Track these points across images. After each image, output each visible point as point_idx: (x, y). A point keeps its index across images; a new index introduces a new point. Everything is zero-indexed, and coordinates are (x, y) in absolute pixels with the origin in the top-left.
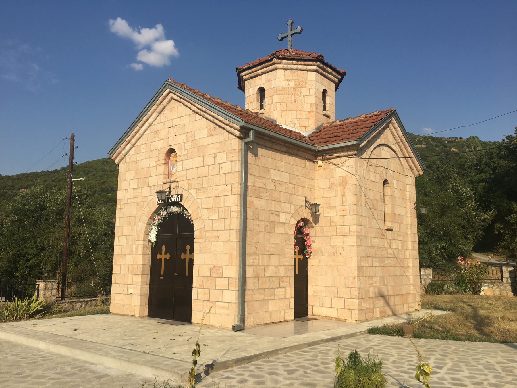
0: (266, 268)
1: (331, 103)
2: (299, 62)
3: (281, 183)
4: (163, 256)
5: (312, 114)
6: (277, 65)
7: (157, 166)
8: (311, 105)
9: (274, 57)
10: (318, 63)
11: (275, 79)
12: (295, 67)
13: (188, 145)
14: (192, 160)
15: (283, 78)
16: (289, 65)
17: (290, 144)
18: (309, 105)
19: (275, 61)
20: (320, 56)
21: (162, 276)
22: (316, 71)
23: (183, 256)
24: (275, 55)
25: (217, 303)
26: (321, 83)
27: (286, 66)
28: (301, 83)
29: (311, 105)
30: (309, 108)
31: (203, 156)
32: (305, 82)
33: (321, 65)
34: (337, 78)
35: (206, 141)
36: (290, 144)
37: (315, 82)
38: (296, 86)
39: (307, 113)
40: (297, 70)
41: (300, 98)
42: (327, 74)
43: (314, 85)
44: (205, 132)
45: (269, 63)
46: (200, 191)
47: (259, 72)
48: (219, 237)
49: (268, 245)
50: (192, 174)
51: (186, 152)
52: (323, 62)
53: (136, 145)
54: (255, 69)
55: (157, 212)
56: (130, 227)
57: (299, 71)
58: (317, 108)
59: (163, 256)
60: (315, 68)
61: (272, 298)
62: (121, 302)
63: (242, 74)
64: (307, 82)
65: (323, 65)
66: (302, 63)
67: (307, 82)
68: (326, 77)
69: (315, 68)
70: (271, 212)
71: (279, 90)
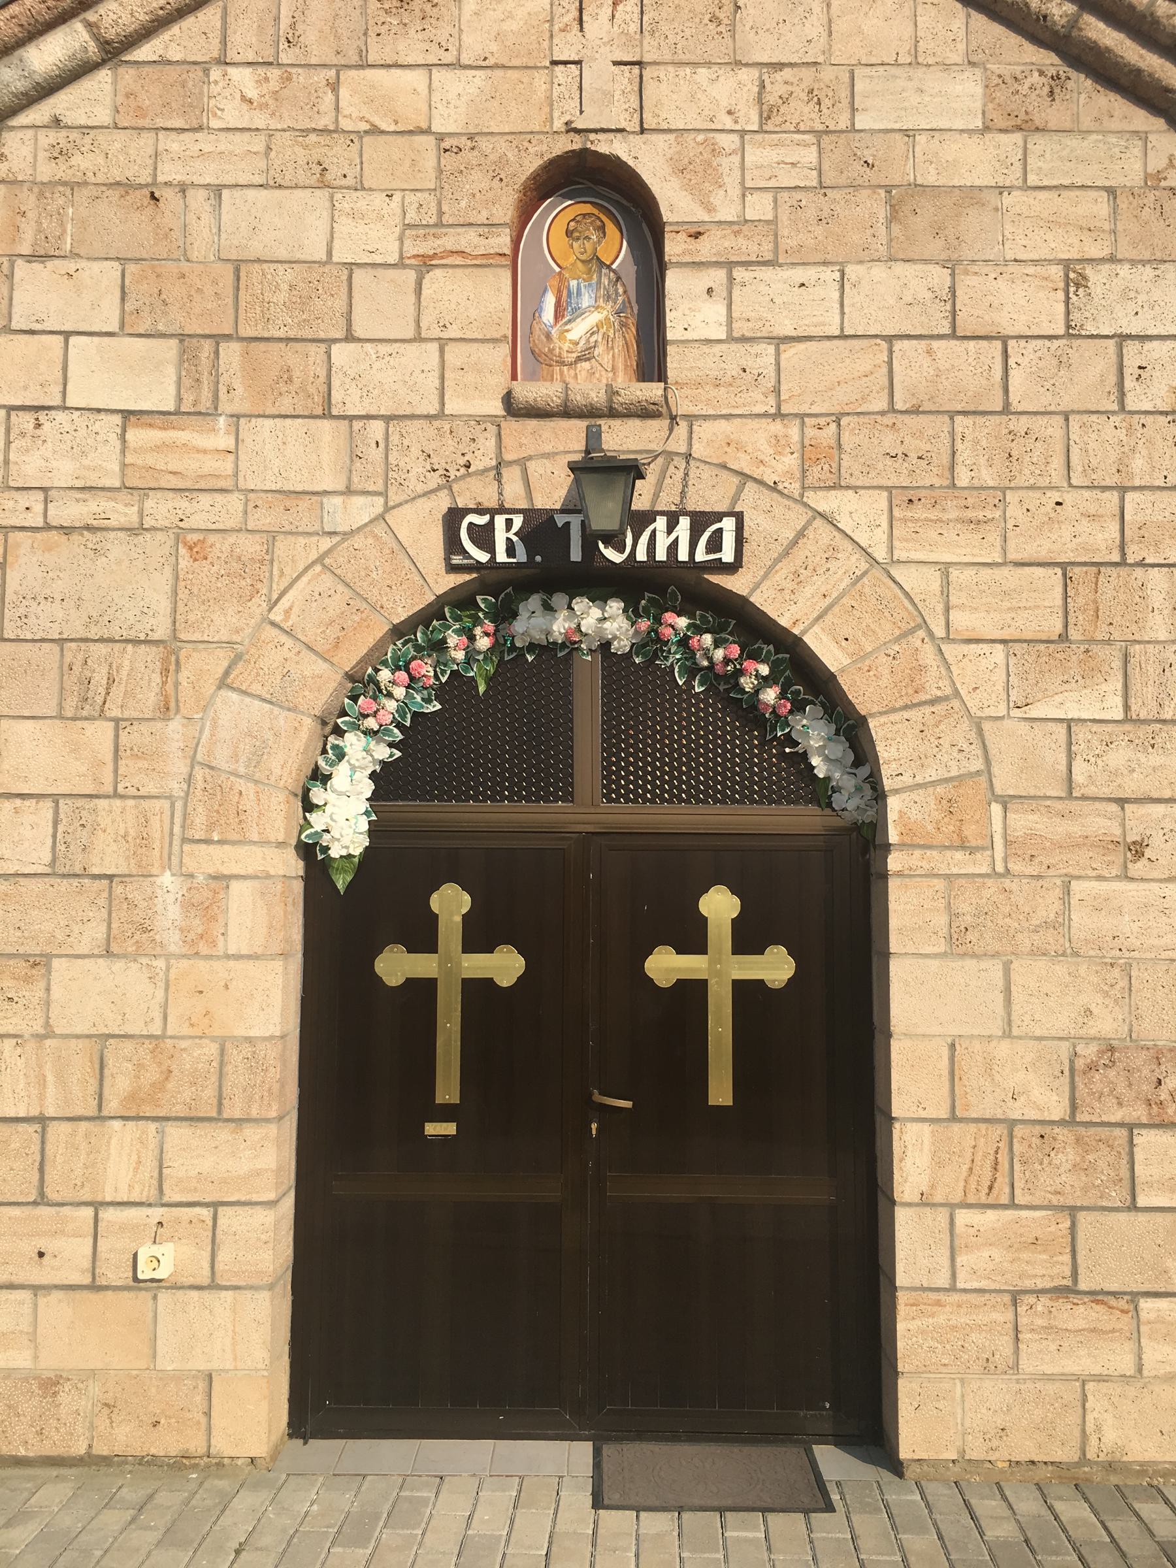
4: (455, 960)
7: (426, 264)
13: (787, 160)
14: (830, 275)
21: (445, 1113)
23: (665, 965)
25: (1145, 1304)
31: (952, 266)
35: (978, 161)
44: (965, 95)
46: (918, 512)
48: (1137, 850)
50: (825, 379)
51: (759, 207)
53: (144, 52)
55: (421, 630)
56: (100, 734)
59: (455, 960)
62: (21, 1359)
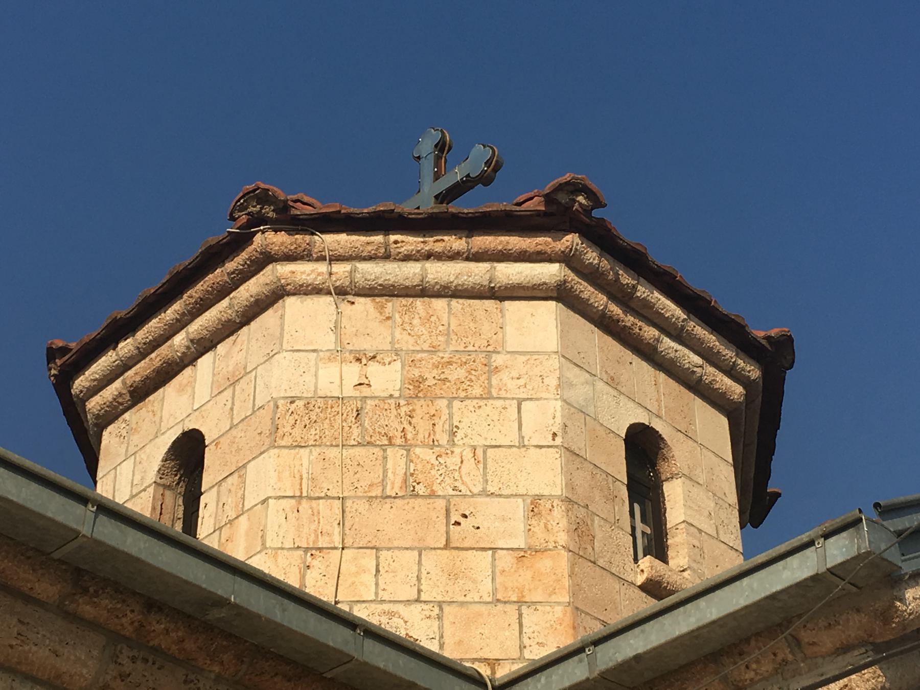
1: (707, 526)
2: (432, 243)
5: (545, 564)
6: (283, 270)
8: (535, 506)
9: (257, 221)
10: (571, 240)
11: (270, 357)
12: (410, 272)
15: (328, 341)
16: (363, 266)
17: (152, 605)
18: (519, 507)
19: (269, 239)
20: (575, 188)
22: (561, 294)
24: (264, 197)
26: (612, 382)
27: (341, 269)
28: (456, 373)
29: (535, 506)
30: (520, 526)
32: (485, 362)
33: (592, 256)
34: (731, 372)
36: (152, 605)
37: (555, 362)
38: (416, 388)
39: (506, 560)
40: (423, 291)
41: (452, 461)
42: (650, 332)
43: (552, 381)
45: (231, 266)
47: (179, 340)
52: (600, 236)
54: (154, 326)
57: (440, 304)
58: (581, 531)
60: (550, 272)
63: (80, 383)
64: (498, 360)
65: (626, 277)
66: (454, 242)
67: (498, 360)
68: (648, 353)
69: (550, 272)
71: (302, 420)
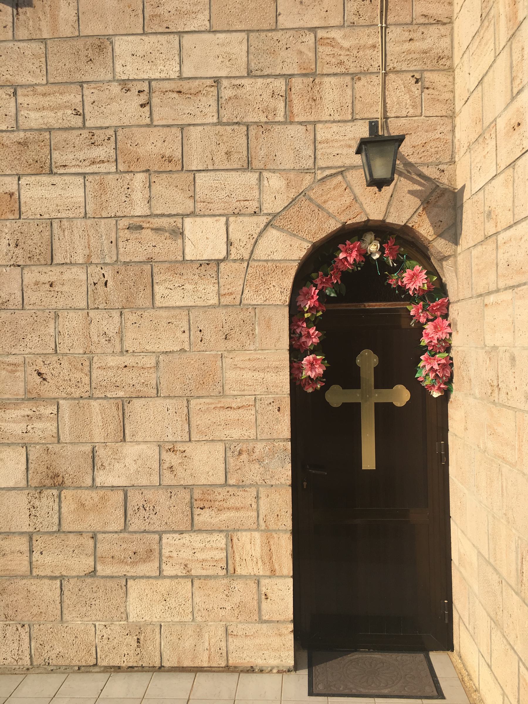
0: (101, 452)
3: (185, 86)
49: (113, 361)
61: (149, 568)
70: (124, 223)
